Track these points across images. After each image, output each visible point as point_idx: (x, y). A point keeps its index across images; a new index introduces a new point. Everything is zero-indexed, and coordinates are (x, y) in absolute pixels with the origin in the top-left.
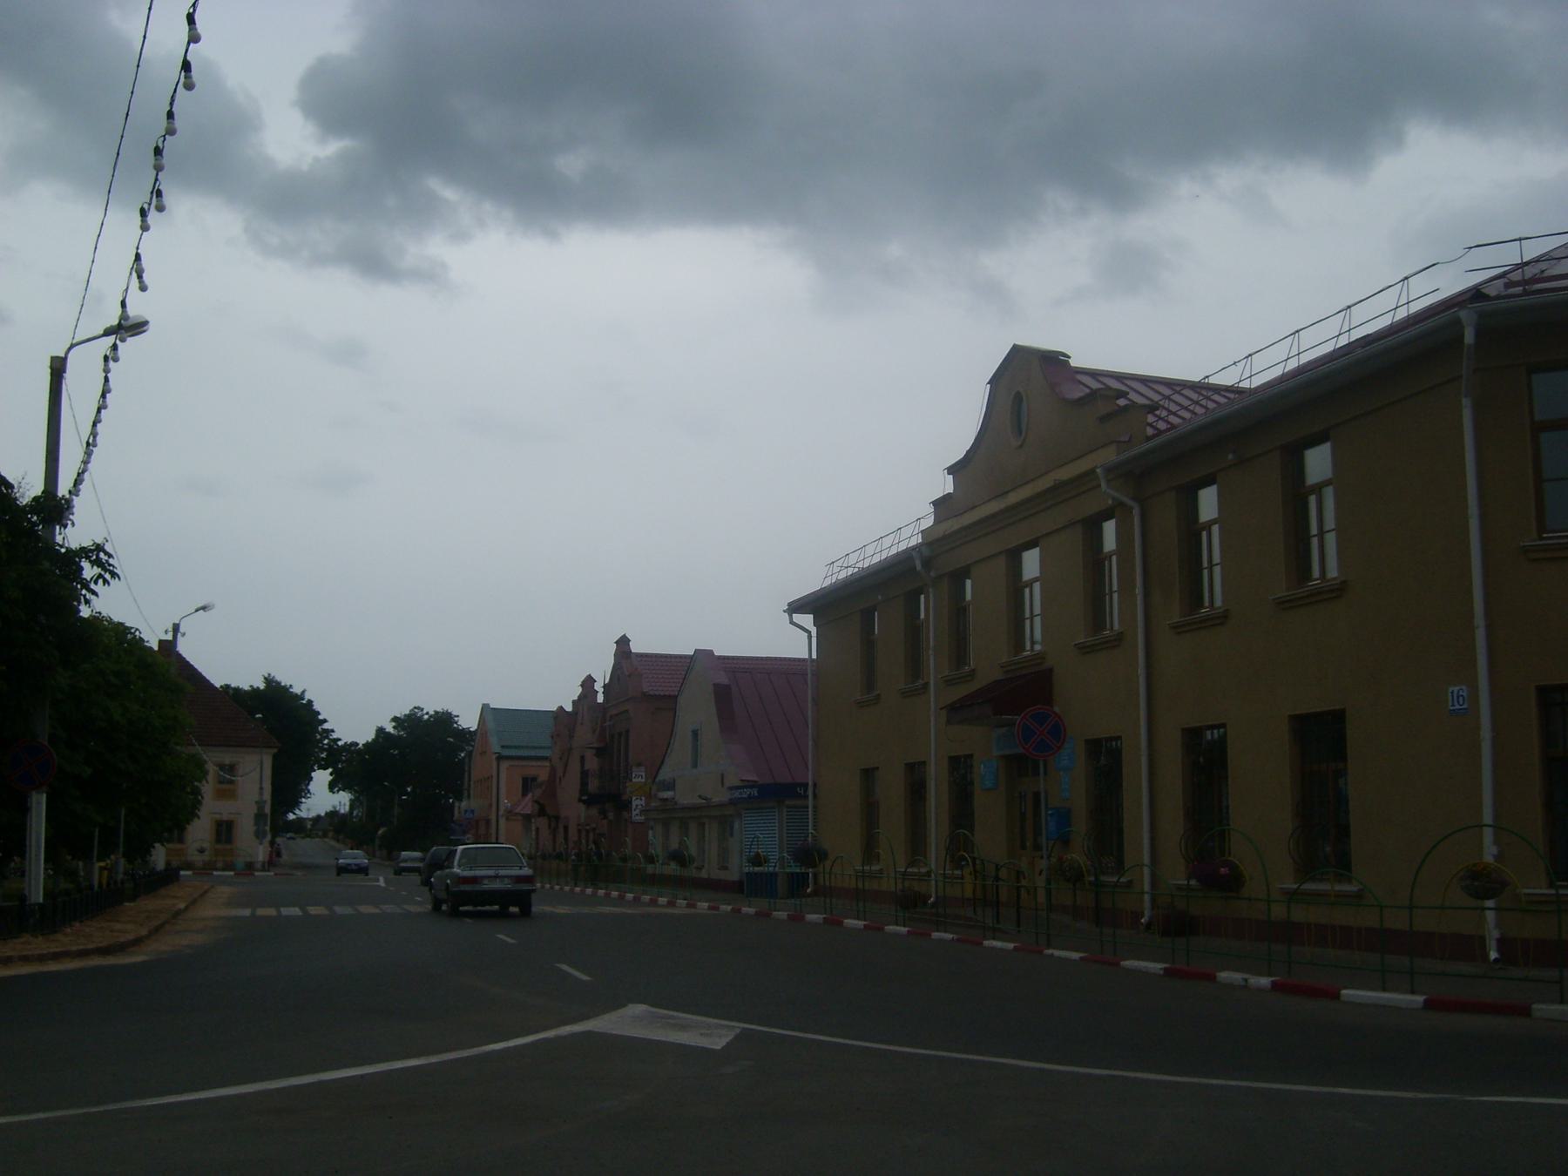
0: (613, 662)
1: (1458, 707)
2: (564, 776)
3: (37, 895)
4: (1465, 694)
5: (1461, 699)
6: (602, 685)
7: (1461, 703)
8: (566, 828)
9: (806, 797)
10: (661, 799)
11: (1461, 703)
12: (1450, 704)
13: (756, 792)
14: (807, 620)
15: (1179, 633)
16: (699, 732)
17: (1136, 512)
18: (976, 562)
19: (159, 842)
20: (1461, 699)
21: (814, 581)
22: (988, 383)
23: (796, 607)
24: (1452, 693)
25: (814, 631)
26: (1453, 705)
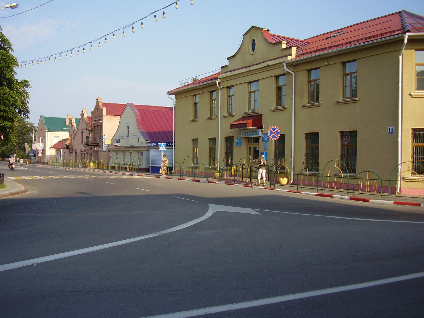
0: (95, 105)
1: (391, 132)
2: (75, 137)
3: (61, 149)
4: (393, 129)
5: (392, 130)
6: (91, 111)
7: (392, 131)
8: (76, 152)
9: (172, 146)
10: (114, 145)
11: (392, 131)
12: (389, 131)
13: (155, 144)
14: (173, 97)
15: (208, 120)
16: (305, 102)
17: (293, 75)
18: (235, 85)
19: (6, 77)
20: (392, 130)
21: (175, 86)
22: (243, 36)
23: (170, 93)
24: (389, 128)
25: (175, 100)
26: (389, 131)
